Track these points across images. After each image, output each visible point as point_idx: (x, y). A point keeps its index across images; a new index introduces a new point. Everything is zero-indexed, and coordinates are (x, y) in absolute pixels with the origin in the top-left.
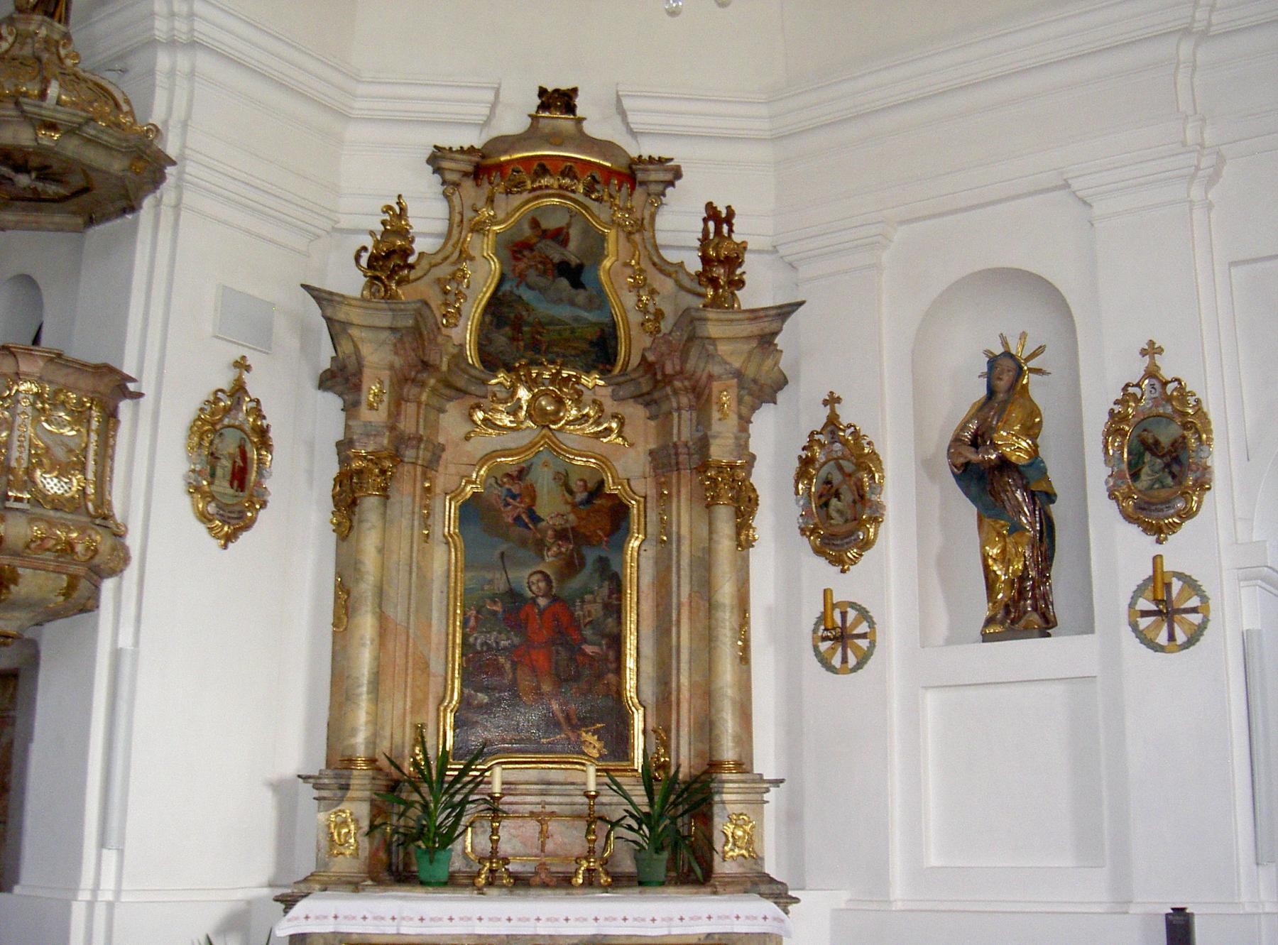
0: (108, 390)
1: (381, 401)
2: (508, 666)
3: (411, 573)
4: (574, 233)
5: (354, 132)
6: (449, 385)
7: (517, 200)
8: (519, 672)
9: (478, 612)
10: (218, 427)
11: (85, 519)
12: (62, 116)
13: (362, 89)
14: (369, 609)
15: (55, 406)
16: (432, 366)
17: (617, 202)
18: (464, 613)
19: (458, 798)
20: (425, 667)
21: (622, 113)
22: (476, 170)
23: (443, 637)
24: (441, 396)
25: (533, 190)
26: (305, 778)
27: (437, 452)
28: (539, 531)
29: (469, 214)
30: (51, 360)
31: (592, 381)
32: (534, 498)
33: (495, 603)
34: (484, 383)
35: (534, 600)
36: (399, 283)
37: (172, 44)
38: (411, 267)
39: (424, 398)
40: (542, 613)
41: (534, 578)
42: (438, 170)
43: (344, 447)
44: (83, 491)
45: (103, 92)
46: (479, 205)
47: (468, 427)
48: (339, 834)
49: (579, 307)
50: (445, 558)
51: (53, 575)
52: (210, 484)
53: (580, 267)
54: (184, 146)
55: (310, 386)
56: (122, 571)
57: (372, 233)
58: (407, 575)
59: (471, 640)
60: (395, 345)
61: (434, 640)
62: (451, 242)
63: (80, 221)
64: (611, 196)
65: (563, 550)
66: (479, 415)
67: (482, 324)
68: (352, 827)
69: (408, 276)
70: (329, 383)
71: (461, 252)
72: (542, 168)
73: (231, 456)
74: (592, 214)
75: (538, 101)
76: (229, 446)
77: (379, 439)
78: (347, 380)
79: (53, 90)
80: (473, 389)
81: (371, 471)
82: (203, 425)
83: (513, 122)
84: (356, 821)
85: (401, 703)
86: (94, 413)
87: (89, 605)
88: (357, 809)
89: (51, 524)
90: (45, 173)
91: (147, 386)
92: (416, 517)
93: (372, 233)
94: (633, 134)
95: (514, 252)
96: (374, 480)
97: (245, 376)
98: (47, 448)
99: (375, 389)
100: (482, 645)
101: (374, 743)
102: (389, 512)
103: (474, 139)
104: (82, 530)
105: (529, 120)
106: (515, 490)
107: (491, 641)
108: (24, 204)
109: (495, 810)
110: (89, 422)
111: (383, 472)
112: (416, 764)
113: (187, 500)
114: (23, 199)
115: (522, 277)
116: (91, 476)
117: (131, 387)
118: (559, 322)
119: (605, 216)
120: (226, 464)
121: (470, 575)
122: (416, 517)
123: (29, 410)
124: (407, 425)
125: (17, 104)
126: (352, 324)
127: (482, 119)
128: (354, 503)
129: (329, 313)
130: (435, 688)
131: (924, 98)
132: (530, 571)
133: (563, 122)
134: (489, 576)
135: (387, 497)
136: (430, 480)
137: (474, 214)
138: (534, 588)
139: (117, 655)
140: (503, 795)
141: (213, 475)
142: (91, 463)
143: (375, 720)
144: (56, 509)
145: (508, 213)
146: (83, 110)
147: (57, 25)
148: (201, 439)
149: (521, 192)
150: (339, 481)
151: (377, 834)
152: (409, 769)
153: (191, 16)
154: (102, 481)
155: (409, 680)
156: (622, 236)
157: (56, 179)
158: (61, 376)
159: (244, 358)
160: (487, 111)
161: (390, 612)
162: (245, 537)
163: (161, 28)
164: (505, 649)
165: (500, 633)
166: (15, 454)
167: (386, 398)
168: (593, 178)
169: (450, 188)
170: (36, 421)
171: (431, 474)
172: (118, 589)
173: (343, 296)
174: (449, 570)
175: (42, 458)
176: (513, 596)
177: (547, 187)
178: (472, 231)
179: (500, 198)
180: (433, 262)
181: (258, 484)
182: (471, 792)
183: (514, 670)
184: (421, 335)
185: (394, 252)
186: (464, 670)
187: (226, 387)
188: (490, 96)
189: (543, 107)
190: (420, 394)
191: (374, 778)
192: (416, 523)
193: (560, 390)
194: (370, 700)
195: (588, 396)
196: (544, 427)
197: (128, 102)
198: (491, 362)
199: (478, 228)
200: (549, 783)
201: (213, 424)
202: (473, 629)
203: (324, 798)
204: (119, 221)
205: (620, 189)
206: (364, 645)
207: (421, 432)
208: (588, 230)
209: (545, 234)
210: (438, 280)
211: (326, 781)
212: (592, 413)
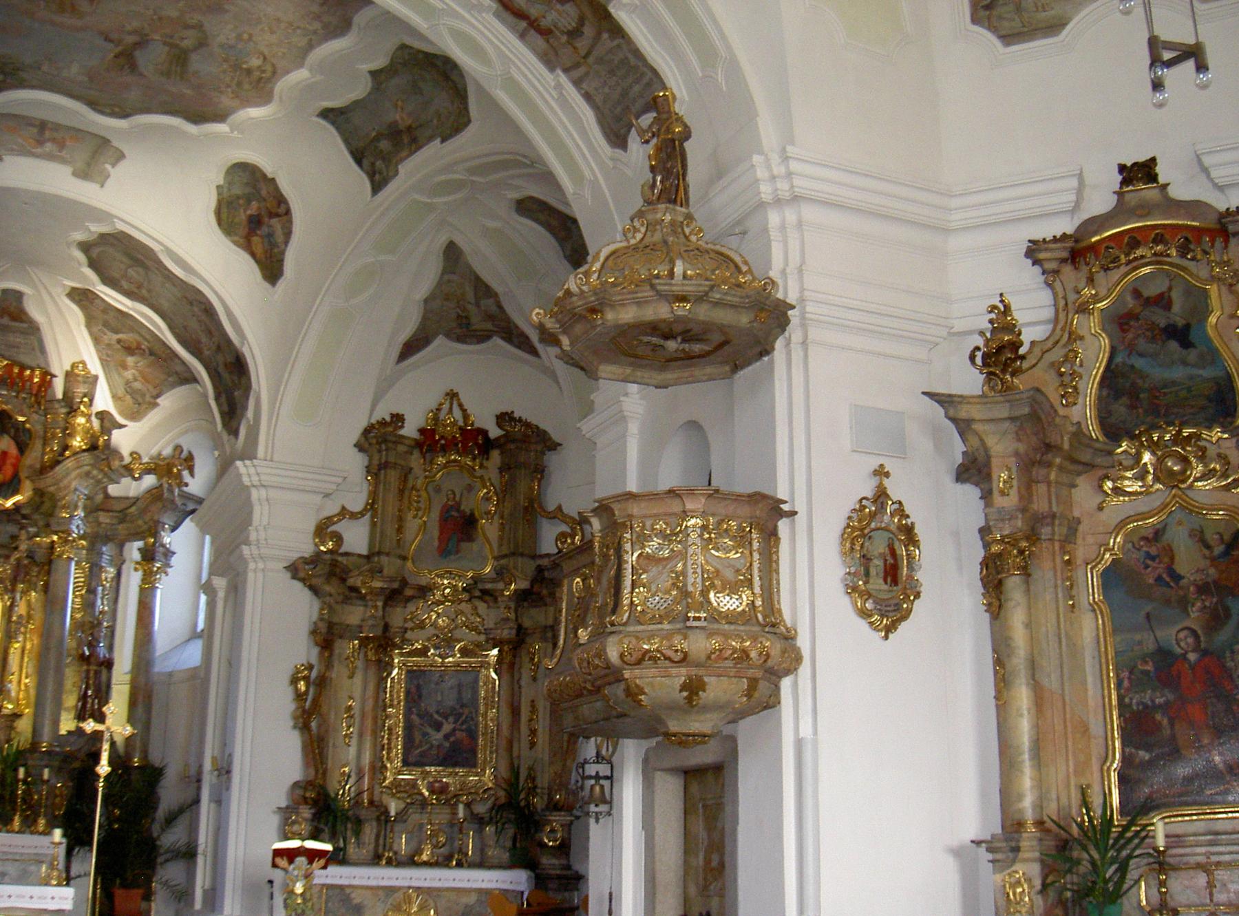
0: (765, 516)
1: (1011, 487)
2: (1165, 722)
3: (1060, 642)
4: (1175, 295)
5: (957, 242)
6: (1074, 461)
7: (1115, 275)
8: (1177, 727)
9: (1131, 673)
10: (866, 531)
11: (756, 629)
12: (690, 288)
13: (955, 203)
14: (1023, 680)
15: (719, 535)
16: (1055, 447)
17: (1212, 258)
18: (1117, 675)
19: (1124, 853)
20: (1085, 729)
21: (1205, 170)
22: (1070, 256)
23: (1100, 698)
24: (1070, 472)
25: (1129, 262)
26: (977, 843)
27: (1073, 526)
28: (1181, 588)
29: (1072, 297)
30: (710, 496)
31: (1217, 434)
32: (1172, 559)
33: (1146, 662)
34: (1110, 453)
35: (1184, 655)
36: (1013, 375)
37: (778, 202)
38: (1023, 358)
39: (1053, 476)
40: (1193, 668)
41: (1181, 635)
42: (1036, 262)
43: (984, 531)
44: (752, 604)
45: (725, 259)
46: (1081, 286)
47: (1099, 499)
48: (1014, 894)
49: (1193, 366)
50: (1093, 625)
51: (735, 680)
52: (865, 583)
53: (1187, 327)
54: (802, 290)
55: (948, 480)
56: (796, 669)
57: (982, 333)
58: (1056, 645)
59: (1127, 700)
60: (1017, 433)
61: (1091, 703)
62: (1059, 327)
63: (727, 368)
64: (1205, 252)
65: (1207, 604)
66: (1109, 485)
67: (1100, 398)
68: (1026, 886)
69: (1020, 367)
70: (966, 476)
71: (1070, 334)
72: (1133, 240)
73: (882, 555)
74: (1191, 275)
75: (1120, 178)
76: (878, 546)
77: (1013, 522)
78: (980, 471)
79: (679, 269)
80: (1099, 460)
81: (1010, 553)
82: (853, 532)
83: (1101, 201)
84: (1029, 881)
85: (1064, 768)
86: (754, 536)
87: (771, 703)
88: (1028, 869)
89: (726, 636)
90: (688, 336)
91: (800, 506)
92: (1060, 590)
93: (982, 333)
94: (1221, 188)
95: (1121, 325)
96: (1014, 559)
97: (886, 482)
98: (717, 571)
99: (1004, 476)
100: (1138, 704)
101: (1042, 808)
102: (1032, 588)
103: (1067, 226)
104: (754, 639)
105: (1116, 197)
106: (1153, 551)
107: (1147, 700)
108: (680, 363)
109: (1161, 865)
110: (750, 543)
111: (1021, 552)
112: (1080, 825)
113: (846, 601)
114: (676, 359)
115: (1131, 349)
116: (757, 590)
117: (785, 507)
118: (1174, 383)
119: (1204, 273)
120: (877, 565)
121: (1118, 639)
122: (1060, 590)
123: (698, 541)
124: (1040, 505)
125: (653, 286)
126: (973, 420)
127: (1070, 206)
128: (1000, 582)
129: (951, 412)
130: (1096, 750)
131: (887, 217)
132: (1180, 627)
133: (1148, 192)
134: (1138, 637)
135: (1029, 575)
136: (1068, 553)
137: (1076, 296)
138: (1182, 644)
139: (799, 744)
140: (1167, 848)
141: (867, 574)
142: (756, 579)
143: (1040, 784)
144: (731, 623)
145: (1108, 290)
146: (707, 279)
147: (678, 208)
148: (853, 544)
149: (1118, 267)
150: (985, 563)
151: (1052, 894)
152: (1075, 830)
153: (789, 175)
154: (770, 593)
155: (1070, 744)
156: (1224, 289)
157: (698, 339)
158: (721, 508)
159: (881, 465)
160: (1073, 197)
161: (1045, 682)
162: (903, 627)
163: (766, 191)
164: (1160, 706)
165: (1154, 690)
166: (691, 580)
167: (1015, 483)
168: (1186, 239)
169: (1051, 276)
170: (705, 549)
171: (1069, 547)
172: (795, 685)
173: (961, 396)
174: (1098, 635)
175: (714, 581)
176: (1163, 655)
177: (1142, 257)
178: (1077, 312)
179: (1100, 277)
180: (1045, 348)
181: (910, 577)
182: (1137, 847)
183: (1172, 725)
184: (1039, 419)
185: (1004, 347)
186: (1123, 730)
187: (869, 494)
188: (1074, 183)
189: (1125, 182)
190: (1049, 474)
191: (1041, 840)
192: (1060, 595)
193: (1183, 449)
194: (1032, 766)
195: (1212, 451)
196: (1173, 487)
197: (746, 263)
198: (1114, 433)
199: (1083, 309)
200: (1217, 833)
201: (862, 530)
202: (1128, 690)
203: (998, 861)
204: (758, 364)
205: (1213, 246)
206: (1021, 715)
207: (1055, 509)
208: (1189, 291)
209: (1149, 302)
210: (1052, 364)
211: (999, 845)
212: (1218, 467)
